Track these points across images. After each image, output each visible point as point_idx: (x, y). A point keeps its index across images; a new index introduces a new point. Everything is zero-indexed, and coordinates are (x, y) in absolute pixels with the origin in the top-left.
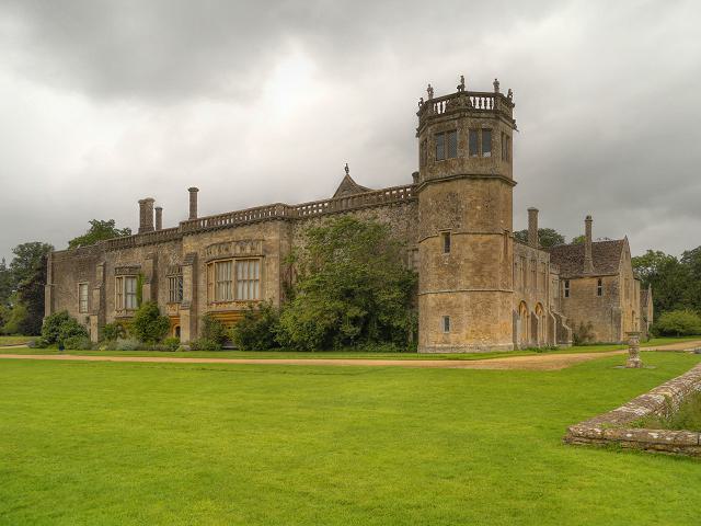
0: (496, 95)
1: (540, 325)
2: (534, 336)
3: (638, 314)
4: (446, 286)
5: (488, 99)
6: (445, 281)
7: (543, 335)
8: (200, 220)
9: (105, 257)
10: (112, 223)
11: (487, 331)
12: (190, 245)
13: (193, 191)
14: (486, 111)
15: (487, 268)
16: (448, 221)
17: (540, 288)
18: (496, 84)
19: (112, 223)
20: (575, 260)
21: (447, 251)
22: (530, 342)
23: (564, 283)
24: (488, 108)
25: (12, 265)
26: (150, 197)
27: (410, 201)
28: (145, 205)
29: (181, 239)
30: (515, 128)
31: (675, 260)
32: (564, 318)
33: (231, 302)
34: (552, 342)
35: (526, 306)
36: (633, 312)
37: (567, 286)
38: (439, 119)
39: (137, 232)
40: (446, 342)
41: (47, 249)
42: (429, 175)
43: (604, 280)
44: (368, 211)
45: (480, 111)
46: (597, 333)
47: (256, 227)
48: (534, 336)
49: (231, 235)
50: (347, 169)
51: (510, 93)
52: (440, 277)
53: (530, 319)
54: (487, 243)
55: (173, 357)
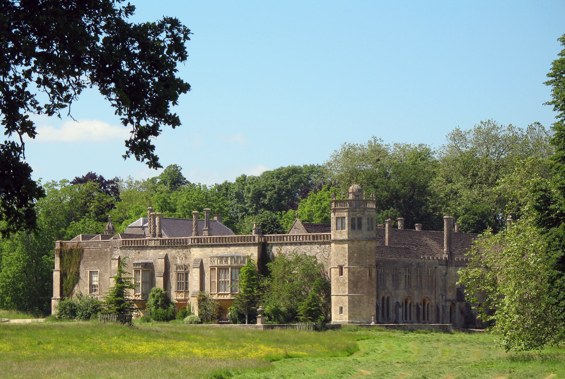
4: (341, 292)
11: (360, 315)
15: (359, 285)
21: (342, 275)
33: (227, 294)
40: (341, 319)
47: (243, 248)
54: (359, 272)
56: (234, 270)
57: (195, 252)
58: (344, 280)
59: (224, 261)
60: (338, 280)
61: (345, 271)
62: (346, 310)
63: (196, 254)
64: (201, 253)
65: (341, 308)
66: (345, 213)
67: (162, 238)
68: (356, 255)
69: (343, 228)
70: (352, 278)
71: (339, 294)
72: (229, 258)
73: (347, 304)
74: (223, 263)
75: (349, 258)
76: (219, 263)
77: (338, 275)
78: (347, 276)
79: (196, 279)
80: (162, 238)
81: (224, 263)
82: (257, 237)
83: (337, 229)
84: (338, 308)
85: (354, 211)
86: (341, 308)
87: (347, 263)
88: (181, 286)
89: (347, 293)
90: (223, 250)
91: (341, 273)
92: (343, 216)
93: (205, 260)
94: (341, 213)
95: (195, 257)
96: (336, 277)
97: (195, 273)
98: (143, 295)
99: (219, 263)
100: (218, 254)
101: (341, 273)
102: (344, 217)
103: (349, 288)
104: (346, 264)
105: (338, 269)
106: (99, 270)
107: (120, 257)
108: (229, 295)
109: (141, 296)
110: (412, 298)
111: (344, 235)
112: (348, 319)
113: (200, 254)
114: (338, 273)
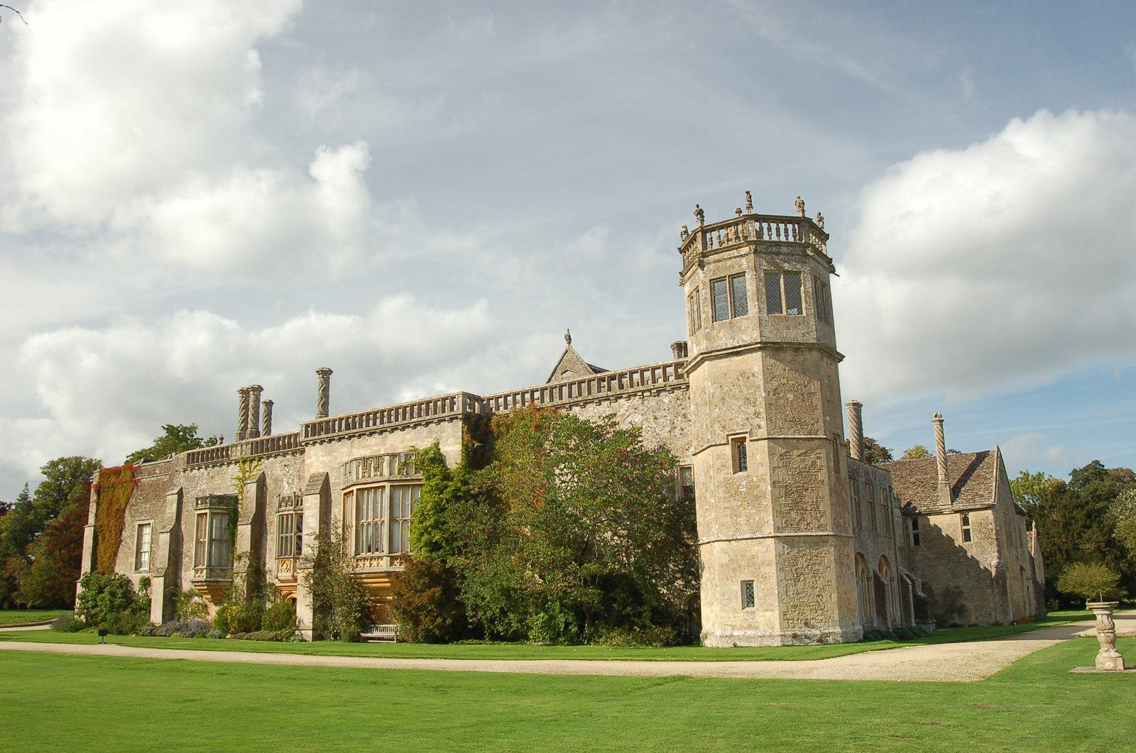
0: (803, 223)
1: (888, 595)
2: (882, 612)
3: (1028, 573)
5: (790, 227)
6: (742, 519)
7: (894, 610)
8: (334, 421)
9: (181, 480)
10: (193, 429)
12: (317, 459)
13: (325, 374)
14: (788, 244)
15: (809, 497)
16: (740, 418)
17: (881, 530)
18: (801, 205)
19: (193, 429)
20: (922, 484)
22: (875, 625)
23: (910, 523)
24: (791, 239)
25: (37, 492)
26: (256, 383)
27: (674, 388)
28: (251, 395)
29: (303, 452)
30: (833, 271)
31: (1063, 484)
32: (919, 581)
34: (908, 620)
35: (863, 559)
36: (1022, 569)
37: (915, 526)
38: (716, 257)
39: (932, 523)
40: (750, 627)
41: (93, 465)
42: (704, 346)
43: (971, 516)
44: (605, 404)
45: (778, 244)
46: (970, 606)
48: (882, 612)
49: (383, 443)
50: (27, 485)
51: (821, 220)
52: (735, 514)
53: (895, 583)
55: (285, 651)
56: (399, 493)
57: (313, 459)
58: (752, 486)
59: (372, 469)
60: (730, 489)
61: (758, 453)
62: (767, 590)
63: (316, 464)
64: (325, 458)
65: (748, 587)
66: (744, 260)
67: (258, 439)
68: (790, 396)
69: (739, 309)
70: (782, 475)
71: (800, 534)
72: (387, 458)
73: (771, 571)
74: (369, 476)
75: (769, 406)
76: (360, 477)
77: (731, 470)
78: (765, 470)
79: (311, 525)
80: (258, 439)
81: (372, 475)
82: (460, 399)
83: (715, 319)
84: (737, 588)
85: (773, 253)
86: (748, 587)
87: (763, 423)
88: (286, 544)
89: (769, 530)
90: (376, 445)
91: (740, 462)
92: (736, 270)
93: (335, 474)
94: (729, 263)
95: (313, 471)
96: (722, 476)
97: (308, 508)
98: (211, 570)
99: (360, 477)
100: (379, 450)
101: (740, 462)
102: (743, 274)
103: (777, 513)
104: (759, 427)
105: (728, 449)
106: (151, 521)
107: (182, 488)
108: (385, 558)
109: (205, 570)
110: (866, 557)
111: (743, 332)
112: (777, 627)
113: (323, 463)
114: (730, 462)
